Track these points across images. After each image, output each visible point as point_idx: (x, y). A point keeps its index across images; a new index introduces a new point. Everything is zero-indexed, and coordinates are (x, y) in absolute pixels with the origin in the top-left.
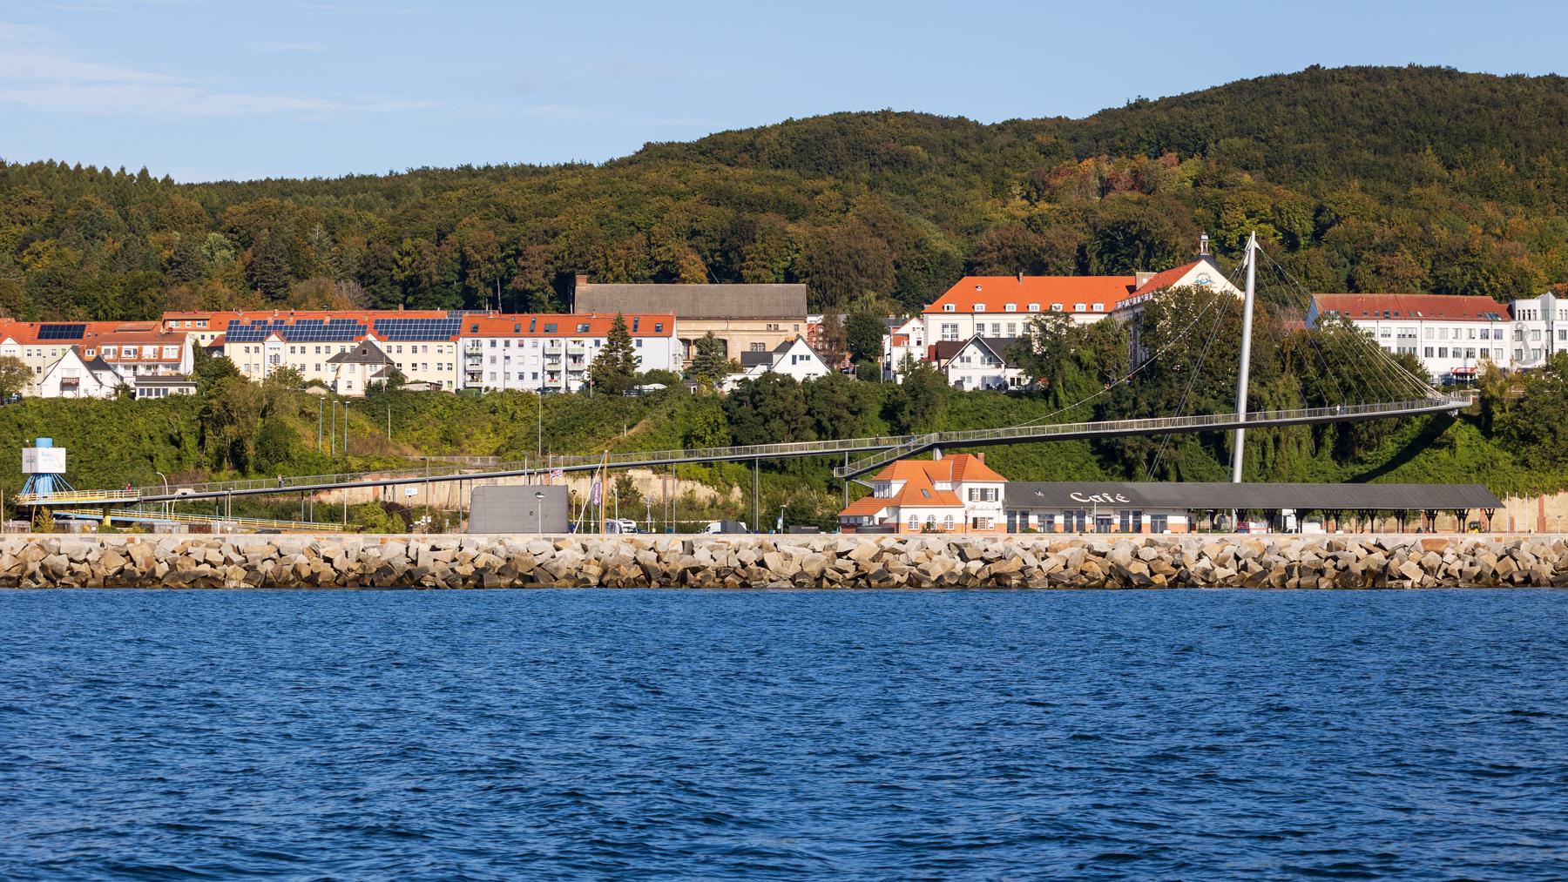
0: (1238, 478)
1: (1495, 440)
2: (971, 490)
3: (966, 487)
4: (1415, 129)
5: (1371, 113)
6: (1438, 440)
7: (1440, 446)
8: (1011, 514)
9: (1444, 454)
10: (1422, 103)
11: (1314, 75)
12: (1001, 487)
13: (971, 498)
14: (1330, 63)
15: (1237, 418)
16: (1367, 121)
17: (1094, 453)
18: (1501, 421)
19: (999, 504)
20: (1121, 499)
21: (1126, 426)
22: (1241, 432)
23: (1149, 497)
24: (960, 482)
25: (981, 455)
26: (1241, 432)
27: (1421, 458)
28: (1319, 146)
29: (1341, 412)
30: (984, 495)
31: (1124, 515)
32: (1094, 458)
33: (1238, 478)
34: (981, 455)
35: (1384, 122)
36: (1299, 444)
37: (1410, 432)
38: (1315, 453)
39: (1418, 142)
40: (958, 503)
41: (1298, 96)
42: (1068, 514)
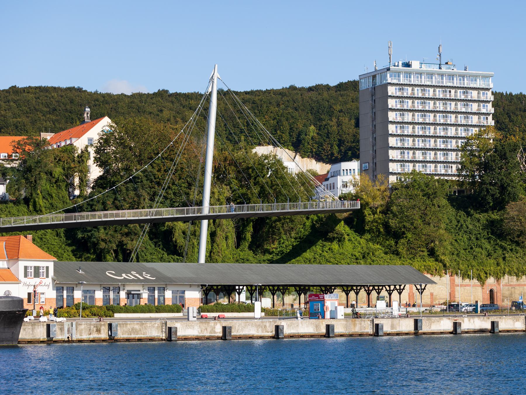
0: (202, 260)
1: (368, 236)
2: (26, 268)
3: (22, 264)
4: (70, 112)
5: (47, 106)
6: (331, 235)
7: (331, 240)
8: (59, 289)
9: (335, 246)
10: (72, 101)
11: (14, 90)
12: (51, 265)
13: (26, 276)
14: (21, 84)
15: (200, 211)
16: (45, 109)
17: (69, 245)
18: (374, 221)
19: (49, 281)
20: (148, 277)
21: (112, 215)
22: (205, 223)
23: (169, 275)
24: (18, 259)
25: (30, 237)
26: (205, 223)
27: (317, 248)
28: (24, 119)
29: (261, 208)
30: (37, 272)
31: (152, 290)
32: (70, 249)
33: (202, 260)
34: (30, 237)
35: (55, 110)
36: (227, 238)
37: (303, 228)
38: (238, 246)
39: (72, 119)
40: (15, 280)
41: (10, 98)
42: (106, 290)
